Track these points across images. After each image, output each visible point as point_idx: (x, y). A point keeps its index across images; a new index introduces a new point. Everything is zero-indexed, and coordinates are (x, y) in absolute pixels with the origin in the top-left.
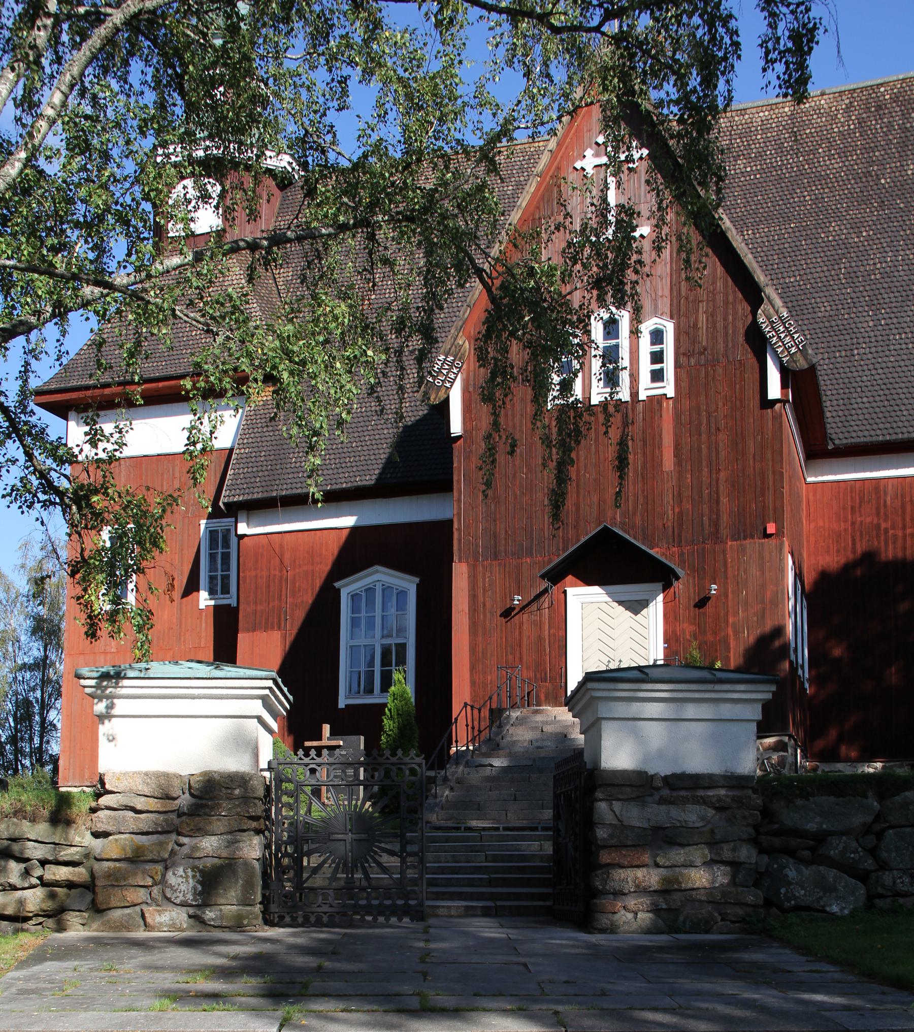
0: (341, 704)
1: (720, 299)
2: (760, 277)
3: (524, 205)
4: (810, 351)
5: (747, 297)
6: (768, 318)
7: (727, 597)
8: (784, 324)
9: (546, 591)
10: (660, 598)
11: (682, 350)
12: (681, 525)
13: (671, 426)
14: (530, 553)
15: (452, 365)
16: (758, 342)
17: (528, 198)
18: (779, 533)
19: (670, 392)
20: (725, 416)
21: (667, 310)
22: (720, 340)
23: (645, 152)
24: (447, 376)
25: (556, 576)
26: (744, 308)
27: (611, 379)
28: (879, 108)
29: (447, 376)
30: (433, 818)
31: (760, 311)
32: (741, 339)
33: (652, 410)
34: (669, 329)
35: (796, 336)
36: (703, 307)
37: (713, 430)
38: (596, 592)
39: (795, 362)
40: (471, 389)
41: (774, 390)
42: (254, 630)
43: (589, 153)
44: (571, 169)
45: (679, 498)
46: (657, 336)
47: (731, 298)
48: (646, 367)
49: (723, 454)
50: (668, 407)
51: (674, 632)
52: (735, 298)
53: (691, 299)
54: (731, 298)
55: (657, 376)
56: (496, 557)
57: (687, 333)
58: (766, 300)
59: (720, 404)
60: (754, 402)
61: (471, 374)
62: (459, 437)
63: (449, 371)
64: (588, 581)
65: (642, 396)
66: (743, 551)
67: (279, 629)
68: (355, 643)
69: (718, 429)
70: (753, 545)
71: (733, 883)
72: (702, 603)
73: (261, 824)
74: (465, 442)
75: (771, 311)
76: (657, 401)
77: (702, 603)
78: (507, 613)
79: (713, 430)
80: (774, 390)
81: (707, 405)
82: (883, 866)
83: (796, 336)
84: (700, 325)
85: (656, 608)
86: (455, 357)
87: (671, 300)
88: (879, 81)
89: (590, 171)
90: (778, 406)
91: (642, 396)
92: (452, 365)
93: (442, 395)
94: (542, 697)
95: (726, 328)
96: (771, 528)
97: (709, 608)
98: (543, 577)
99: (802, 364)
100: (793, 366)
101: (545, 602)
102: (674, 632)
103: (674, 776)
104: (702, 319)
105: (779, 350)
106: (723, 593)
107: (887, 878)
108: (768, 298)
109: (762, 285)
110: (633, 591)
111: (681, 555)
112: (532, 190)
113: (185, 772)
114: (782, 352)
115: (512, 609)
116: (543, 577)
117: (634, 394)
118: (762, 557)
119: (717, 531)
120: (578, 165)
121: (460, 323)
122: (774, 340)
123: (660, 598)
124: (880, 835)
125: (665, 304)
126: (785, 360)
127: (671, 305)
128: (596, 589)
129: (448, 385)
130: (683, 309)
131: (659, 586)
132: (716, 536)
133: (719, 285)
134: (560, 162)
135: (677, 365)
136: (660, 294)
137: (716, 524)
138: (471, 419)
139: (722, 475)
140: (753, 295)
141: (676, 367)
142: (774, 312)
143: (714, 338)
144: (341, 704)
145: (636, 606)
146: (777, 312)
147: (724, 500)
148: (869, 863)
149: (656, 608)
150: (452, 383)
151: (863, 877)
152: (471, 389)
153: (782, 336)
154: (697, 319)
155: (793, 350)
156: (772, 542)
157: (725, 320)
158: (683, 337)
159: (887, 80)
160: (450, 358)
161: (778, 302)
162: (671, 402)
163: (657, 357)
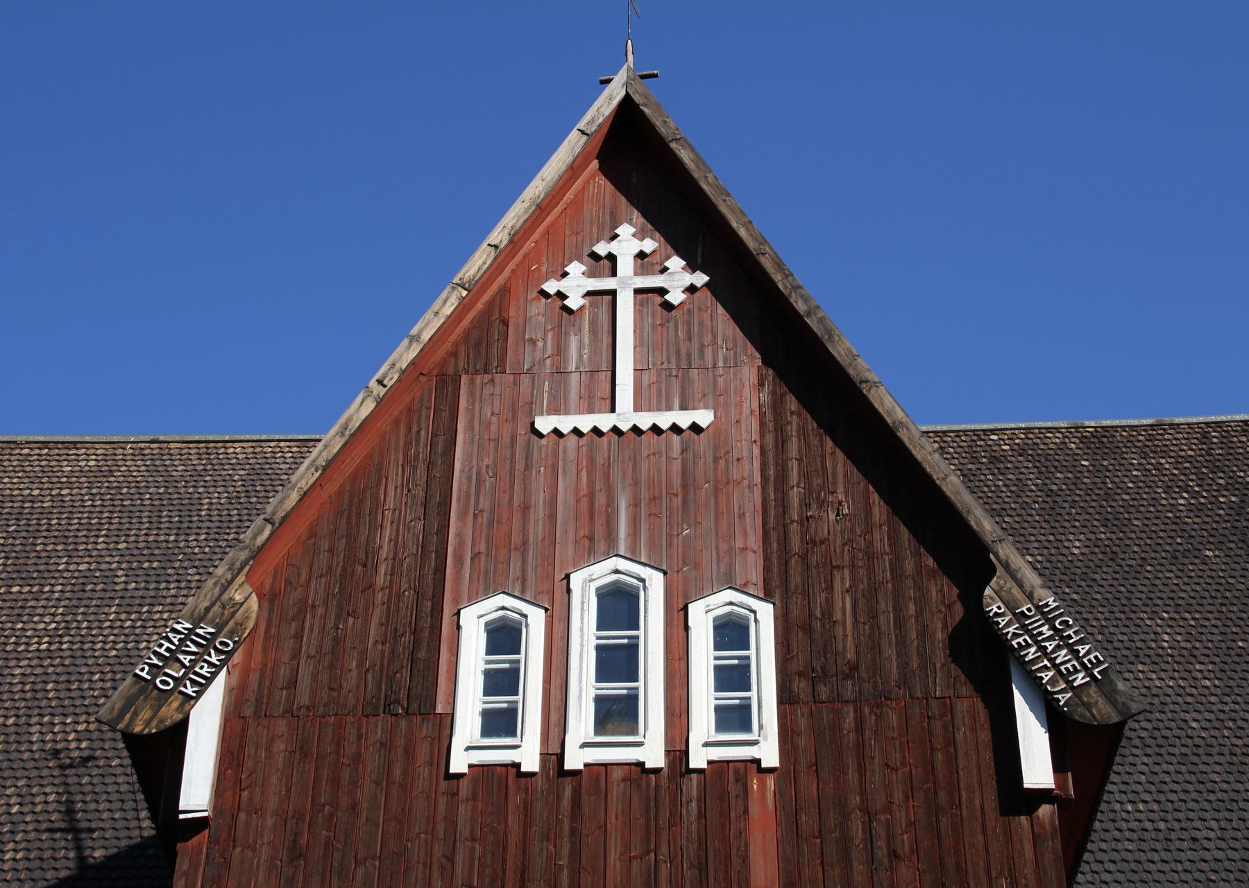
0: (459, 763)
1: (883, 570)
2: (985, 524)
3: (426, 336)
4: (1121, 686)
5: (946, 567)
6: (1011, 606)
8: (1050, 622)
11: (798, 664)
13: (771, 835)
15: (209, 643)
16: (987, 663)
17: (437, 324)
19: (769, 754)
20: (912, 824)
21: (755, 574)
22: (890, 651)
23: (700, 279)
24: (189, 669)
26: (942, 592)
27: (617, 714)
28: (994, 460)
29: (189, 669)
31: (988, 591)
32: (940, 656)
33: (723, 797)
35: (1083, 649)
36: (842, 580)
37: (881, 852)
39: (1088, 706)
40: (248, 712)
41: (1038, 769)
43: (576, 269)
44: (533, 294)
46: (731, 632)
47: (909, 566)
48: (704, 698)
50: (764, 793)
52: (919, 567)
53: (813, 560)
54: (909, 566)
55: (735, 718)
57: (808, 629)
58: (1000, 570)
59: (898, 796)
60: (982, 796)
61: (254, 678)
62: (199, 824)
63: (198, 658)
65: (698, 759)
69: (894, 854)
74: (213, 841)
75: (1016, 592)
79: (881, 852)
80: (1038, 769)
81: (863, 791)
83: (1083, 649)
84: (838, 616)
86: (220, 628)
87: (767, 559)
88: (991, 426)
89: (574, 302)
90: (1045, 810)
91: (698, 759)
92: (209, 643)
93: (170, 713)
95: (900, 624)
99: (1104, 712)
100: (1080, 714)
104: (844, 606)
105: (1047, 676)
108: (1007, 566)
109: (988, 538)
112: (448, 310)
114: (1052, 681)
117: (678, 752)
120: (551, 287)
121: (243, 555)
122: (1031, 653)
125: (752, 567)
126: (1063, 698)
127: (767, 569)
129: (190, 690)
130: (796, 579)
133: (880, 540)
134: (509, 279)
135: (786, 697)
136: (739, 544)
138: (238, 786)
140: (969, 562)
141: (780, 702)
142: (1020, 595)
143: (875, 647)
144: (459, 763)
146: (1030, 597)
150: (202, 688)
152: (248, 712)
153: (1050, 646)
154: (830, 602)
155: (1080, 679)
157: (898, 609)
158: (798, 638)
159: (999, 426)
160: (206, 630)
161: (1031, 578)
162: (770, 781)
163: (733, 677)
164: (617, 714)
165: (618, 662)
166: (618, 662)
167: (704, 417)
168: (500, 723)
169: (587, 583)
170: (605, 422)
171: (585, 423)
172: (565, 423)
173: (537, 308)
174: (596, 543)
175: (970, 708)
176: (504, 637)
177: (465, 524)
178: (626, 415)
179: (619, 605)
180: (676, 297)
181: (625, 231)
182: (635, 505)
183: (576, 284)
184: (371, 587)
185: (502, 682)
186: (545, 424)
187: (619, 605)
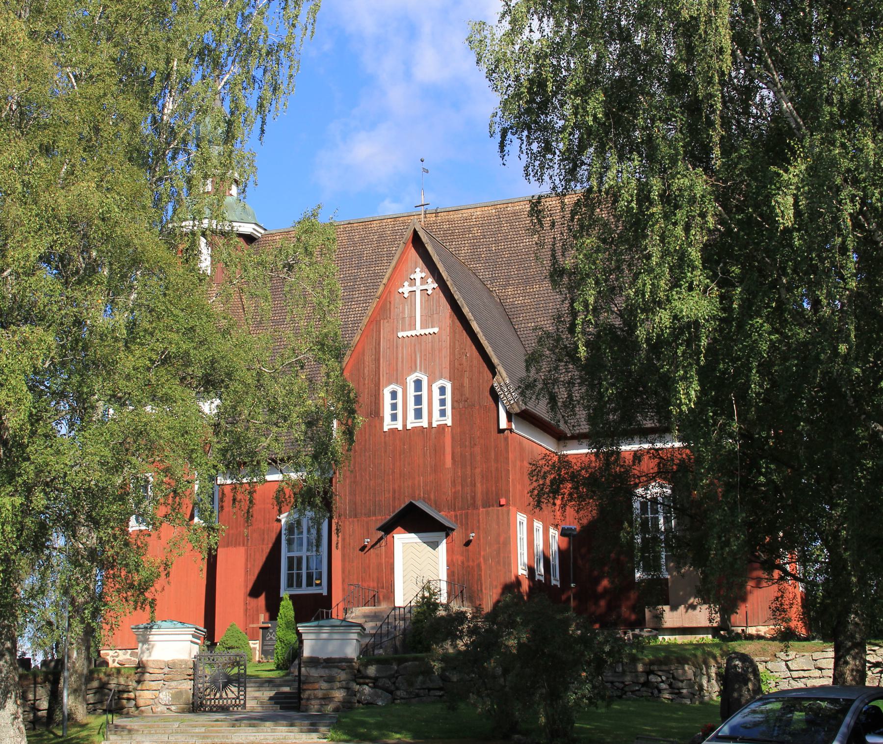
0: (386, 429)
2: (495, 360)
7: (479, 540)
9: (381, 538)
10: (445, 541)
12: (455, 499)
14: (375, 514)
18: (508, 504)
19: (449, 423)
25: (388, 528)
30: (651, 657)
34: (449, 386)
36: (467, 374)
38: (412, 537)
42: (228, 546)
43: (406, 284)
45: (454, 483)
46: (442, 390)
48: (411, 415)
49: (478, 458)
51: (452, 561)
55: (443, 413)
56: (356, 516)
64: (410, 530)
65: (434, 425)
66: (488, 513)
67: (244, 545)
68: (291, 554)
70: (494, 510)
71: (347, 695)
72: (468, 543)
73: (192, 677)
76: (442, 428)
77: (468, 543)
78: (363, 549)
82: (398, 689)
85: (443, 547)
91: (434, 425)
94: (381, 597)
96: (503, 501)
97: (471, 547)
98: (379, 529)
101: (383, 542)
102: (452, 561)
103: (328, 659)
104: (466, 381)
106: (478, 537)
107: (398, 693)
110: (432, 536)
111: (456, 516)
113: (166, 660)
115: (365, 546)
116: (379, 529)
117: (430, 423)
118: (498, 517)
119: (475, 502)
120: (400, 290)
123: (445, 541)
124: (397, 678)
125: (446, 372)
128: (413, 535)
131: (444, 534)
132: (474, 506)
133: (475, 362)
135: (453, 408)
137: (474, 498)
139: (478, 471)
144: (386, 429)
145: (434, 545)
147: (479, 485)
148: (393, 688)
149: (443, 547)
151: (391, 693)
156: (504, 508)
161: (504, 374)
163: (443, 402)
164: (418, 414)
165: (418, 400)
166: (418, 400)
167: (436, 330)
168: (394, 417)
169: (410, 380)
170: (413, 333)
171: (409, 333)
172: (405, 334)
173: (397, 296)
174: (413, 370)
175: (494, 405)
176: (394, 395)
177: (123, 728)
178: (419, 331)
179: (418, 384)
180: (430, 292)
181: (418, 270)
182: (421, 357)
183: (406, 289)
184: (404, 318)
185: (394, 407)
186: (400, 334)
187: (418, 384)
